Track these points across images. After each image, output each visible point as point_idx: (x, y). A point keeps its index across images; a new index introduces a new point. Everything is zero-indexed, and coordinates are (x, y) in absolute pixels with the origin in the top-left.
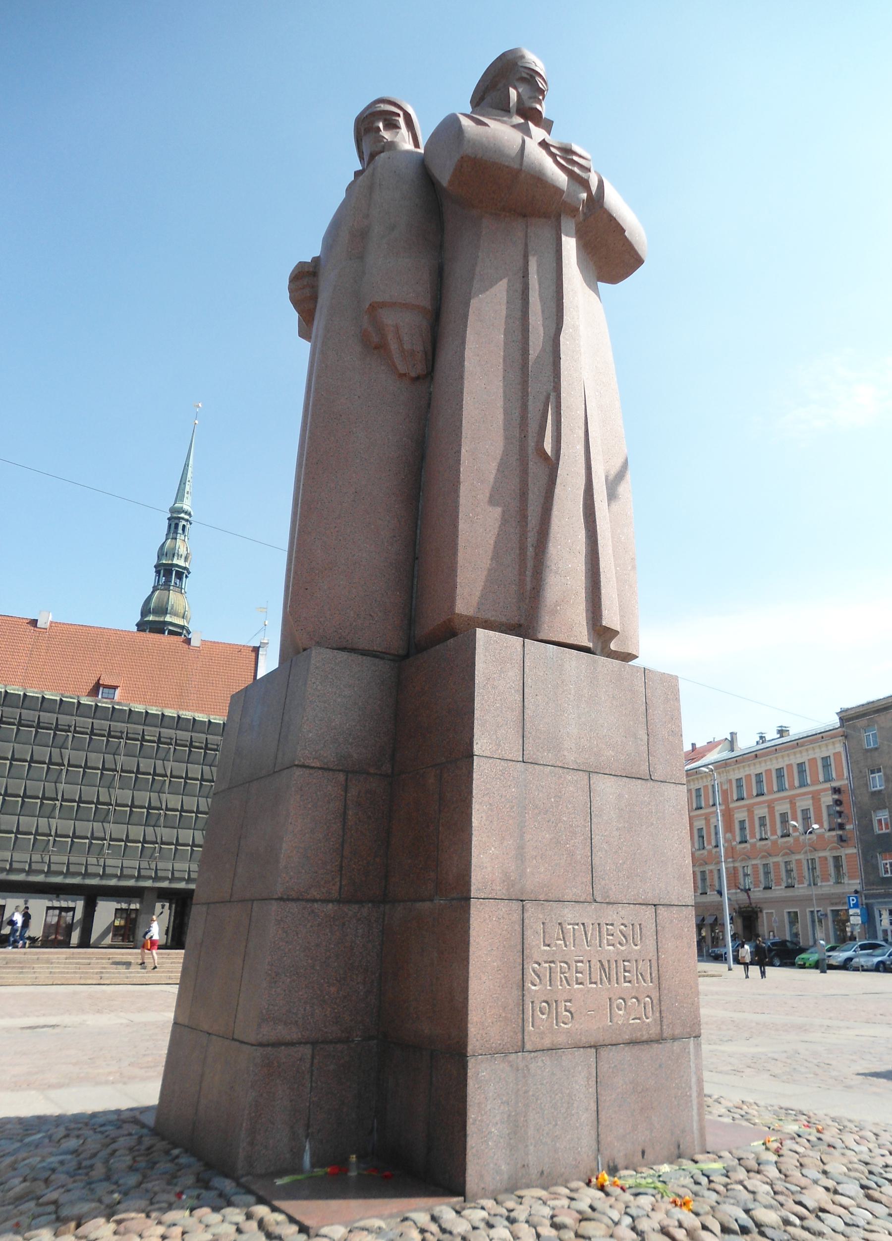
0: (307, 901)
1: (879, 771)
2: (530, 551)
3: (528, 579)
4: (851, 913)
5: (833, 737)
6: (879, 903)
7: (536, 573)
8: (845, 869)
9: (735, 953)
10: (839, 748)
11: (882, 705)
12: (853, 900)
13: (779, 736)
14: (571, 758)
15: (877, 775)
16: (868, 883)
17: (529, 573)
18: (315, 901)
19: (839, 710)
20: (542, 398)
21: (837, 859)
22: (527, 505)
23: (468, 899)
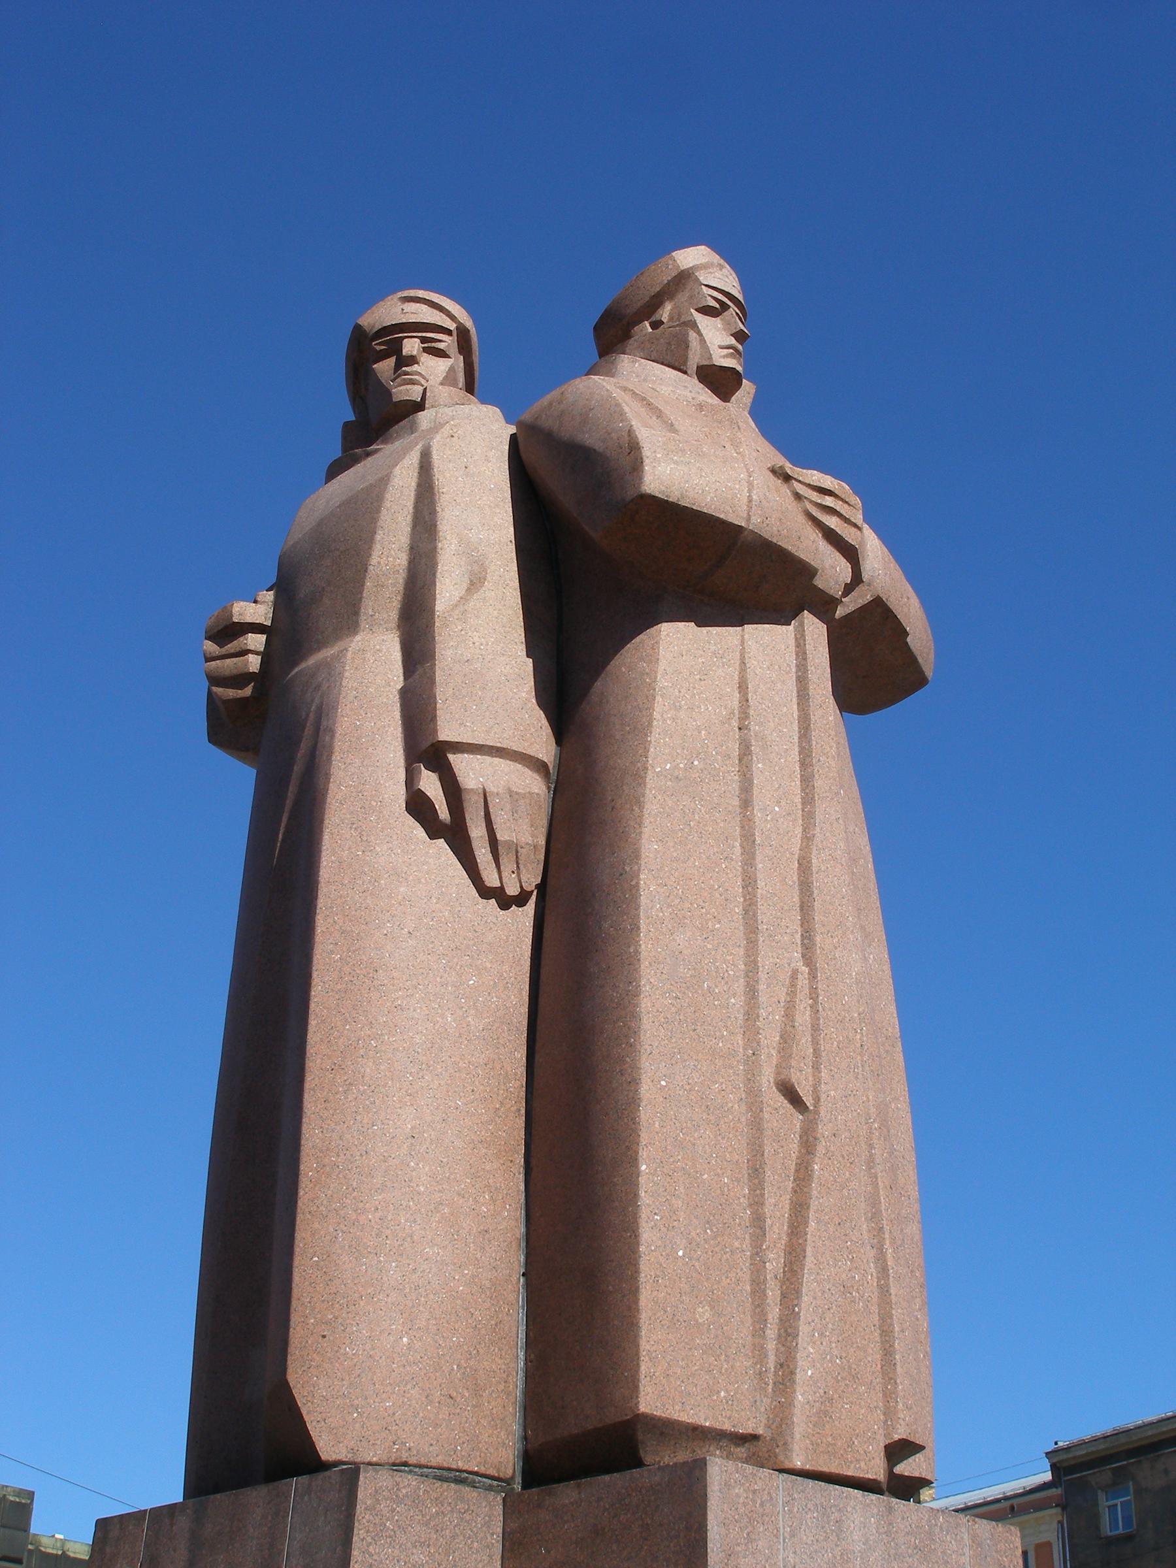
2: (773, 1293)
5: (1039, 1506)
7: (784, 1335)
11: (1147, 1438)
17: (771, 1332)
20: (785, 977)
22: (763, 1195)
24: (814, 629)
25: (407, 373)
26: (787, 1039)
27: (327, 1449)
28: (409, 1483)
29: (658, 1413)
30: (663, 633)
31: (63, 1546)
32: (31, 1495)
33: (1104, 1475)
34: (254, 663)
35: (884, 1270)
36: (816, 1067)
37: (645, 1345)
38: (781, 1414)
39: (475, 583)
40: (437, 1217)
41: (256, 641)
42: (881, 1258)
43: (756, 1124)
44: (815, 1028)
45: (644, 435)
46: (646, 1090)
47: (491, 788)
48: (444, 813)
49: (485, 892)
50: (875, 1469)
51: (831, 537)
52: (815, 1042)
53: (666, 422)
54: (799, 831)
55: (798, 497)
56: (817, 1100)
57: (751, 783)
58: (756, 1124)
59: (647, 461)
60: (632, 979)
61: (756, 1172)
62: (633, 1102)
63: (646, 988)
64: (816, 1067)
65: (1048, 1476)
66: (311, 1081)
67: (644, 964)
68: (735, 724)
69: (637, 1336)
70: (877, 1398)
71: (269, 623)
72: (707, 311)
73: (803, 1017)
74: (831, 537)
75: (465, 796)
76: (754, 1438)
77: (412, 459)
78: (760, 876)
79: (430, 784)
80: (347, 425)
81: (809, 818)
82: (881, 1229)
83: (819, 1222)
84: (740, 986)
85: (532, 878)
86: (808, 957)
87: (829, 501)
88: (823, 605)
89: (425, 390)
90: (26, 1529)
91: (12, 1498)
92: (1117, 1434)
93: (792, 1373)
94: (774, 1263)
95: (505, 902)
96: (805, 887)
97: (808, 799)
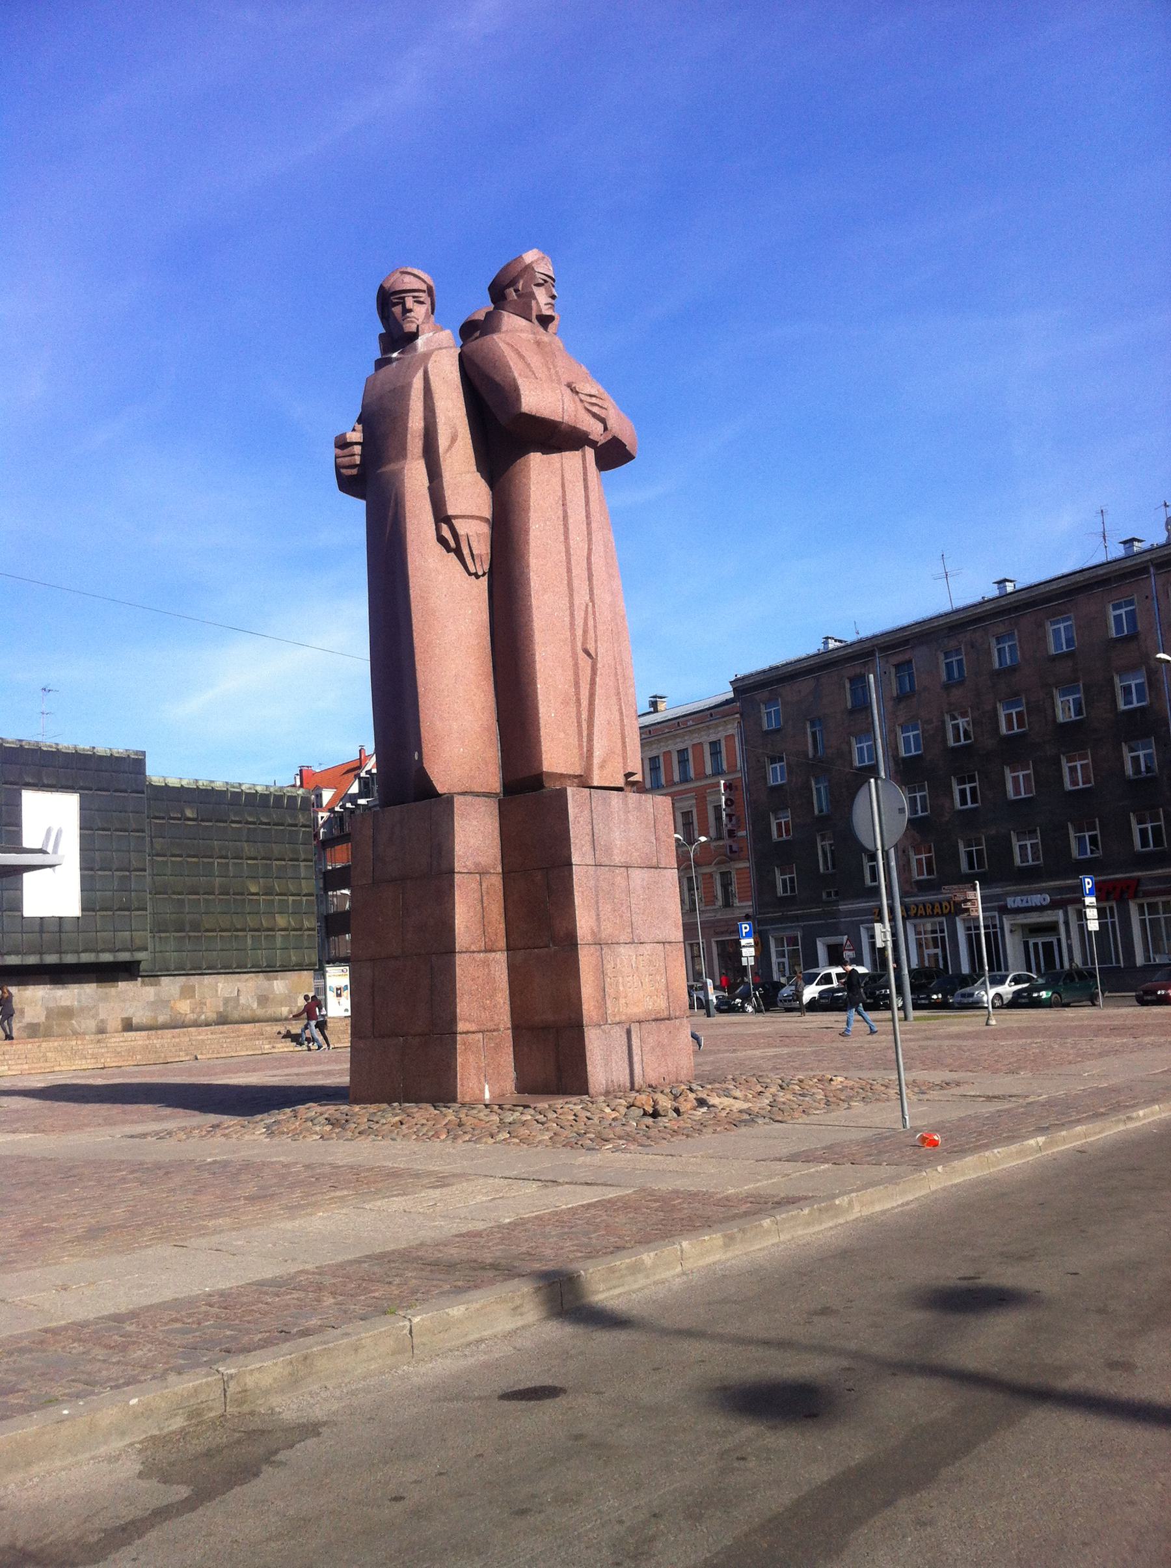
0: (471, 952)
1: (781, 760)
2: (585, 725)
3: (585, 744)
4: (743, 944)
6: (773, 929)
8: (734, 888)
9: (890, 902)
10: (732, 729)
12: (746, 928)
13: (652, 709)
14: (618, 859)
15: (778, 765)
16: (760, 905)
17: (585, 740)
18: (474, 952)
19: (734, 678)
20: (583, 607)
21: (725, 875)
23: (577, 944)
24: (590, 452)
25: (409, 317)
26: (585, 632)
27: (440, 789)
28: (469, 798)
29: (549, 771)
30: (532, 458)
31: (165, 780)
32: (144, 753)
33: (764, 694)
34: (357, 460)
35: (621, 714)
36: (596, 641)
37: (544, 749)
38: (589, 768)
39: (454, 440)
40: (467, 704)
41: (357, 449)
42: (620, 709)
43: (576, 665)
44: (595, 627)
45: (521, 382)
46: (538, 658)
47: (470, 534)
48: (453, 544)
49: (470, 574)
50: (620, 782)
51: (595, 415)
52: (595, 632)
53: (526, 362)
54: (587, 546)
55: (581, 401)
56: (597, 655)
57: (568, 529)
58: (576, 665)
59: (522, 396)
60: (530, 616)
61: (577, 684)
62: (534, 662)
63: (535, 619)
64: (596, 641)
65: (731, 695)
66: (418, 657)
67: (534, 609)
68: (561, 502)
69: (540, 745)
70: (621, 760)
71: (362, 441)
72: (539, 285)
73: (591, 623)
74: (595, 415)
75: (460, 538)
76: (581, 776)
77: (420, 374)
78: (573, 568)
79: (446, 532)
80: (381, 335)
81: (590, 541)
82: (620, 699)
83: (599, 699)
84: (568, 613)
85: (486, 567)
86: (592, 599)
87: (594, 400)
88: (593, 444)
89: (418, 326)
90: (144, 773)
91: (133, 757)
92: (771, 669)
93: (592, 753)
94: (584, 716)
95: (477, 576)
96: (589, 569)
97: (589, 534)
